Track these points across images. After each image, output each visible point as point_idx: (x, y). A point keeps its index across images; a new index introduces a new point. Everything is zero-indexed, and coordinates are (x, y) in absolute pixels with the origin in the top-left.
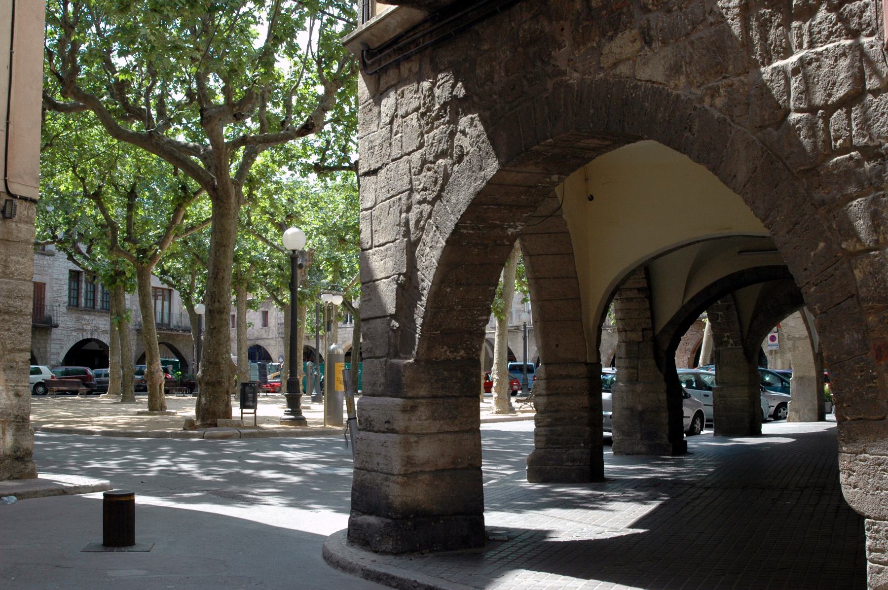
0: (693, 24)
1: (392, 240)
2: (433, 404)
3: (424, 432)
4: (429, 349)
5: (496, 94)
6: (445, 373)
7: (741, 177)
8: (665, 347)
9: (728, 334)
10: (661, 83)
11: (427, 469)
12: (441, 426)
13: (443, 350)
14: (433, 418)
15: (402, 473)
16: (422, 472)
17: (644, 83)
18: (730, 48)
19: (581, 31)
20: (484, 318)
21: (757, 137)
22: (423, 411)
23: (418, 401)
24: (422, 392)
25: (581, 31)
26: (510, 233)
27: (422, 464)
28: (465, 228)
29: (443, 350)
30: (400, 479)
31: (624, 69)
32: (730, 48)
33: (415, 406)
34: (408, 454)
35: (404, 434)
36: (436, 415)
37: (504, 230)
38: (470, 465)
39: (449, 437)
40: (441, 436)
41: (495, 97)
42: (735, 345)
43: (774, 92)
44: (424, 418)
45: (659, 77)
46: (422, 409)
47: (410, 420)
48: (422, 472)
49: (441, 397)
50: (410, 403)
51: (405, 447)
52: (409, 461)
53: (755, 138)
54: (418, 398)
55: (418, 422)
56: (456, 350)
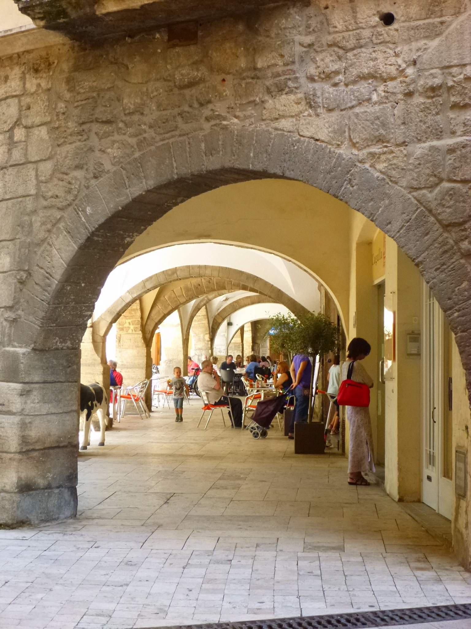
0: (359, 100)
1: (10, 239)
2: (44, 389)
3: (36, 413)
4: (46, 338)
5: (145, 124)
6: (54, 361)
7: (396, 225)
8: (102, 333)
9: (130, 321)
10: (323, 141)
11: (37, 448)
12: (49, 409)
13: (55, 341)
14: (44, 401)
15: (18, 451)
16: (34, 450)
17: (307, 139)
18: (392, 124)
19: (244, 86)
20: (89, 313)
21: (413, 196)
22: (36, 395)
23: (32, 386)
24: (36, 379)
25: (244, 86)
26: (126, 242)
27: (34, 443)
28: (98, 236)
29: (55, 341)
30: (17, 456)
31: (285, 124)
32: (392, 124)
33: (30, 391)
34: (23, 434)
35: (20, 415)
36: (45, 398)
37: (123, 239)
38: (69, 443)
39: (54, 417)
40: (49, 417)
41: (143, 127)
42: (135, 331)
43: (200, 137)
44: (37, 401)
45: (323, 135)
46: (35, 393)
47: (26, 403)
48: (34, 450)
49: (50, 383)
50: (27, 387)
51: (21, 427)
52: (24, 440)
53: (410, 196)
54: (32, 383)
55: (32, 405)
56: (64, 341)
